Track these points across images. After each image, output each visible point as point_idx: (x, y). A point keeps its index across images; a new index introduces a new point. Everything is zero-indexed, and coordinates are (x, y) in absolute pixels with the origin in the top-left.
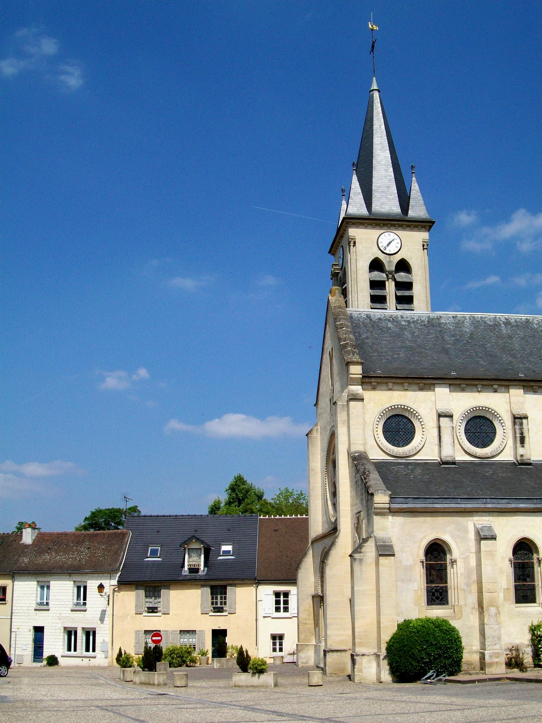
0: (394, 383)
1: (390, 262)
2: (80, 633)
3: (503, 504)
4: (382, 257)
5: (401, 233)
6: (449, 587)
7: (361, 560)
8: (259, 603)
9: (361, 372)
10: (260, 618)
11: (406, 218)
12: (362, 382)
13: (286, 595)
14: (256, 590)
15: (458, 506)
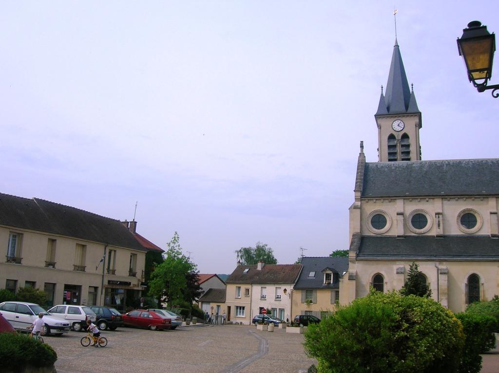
2: (278, 310)
5: (404, 119)
7: (343, 281)
11: (390, 113)
15: (389, 258)
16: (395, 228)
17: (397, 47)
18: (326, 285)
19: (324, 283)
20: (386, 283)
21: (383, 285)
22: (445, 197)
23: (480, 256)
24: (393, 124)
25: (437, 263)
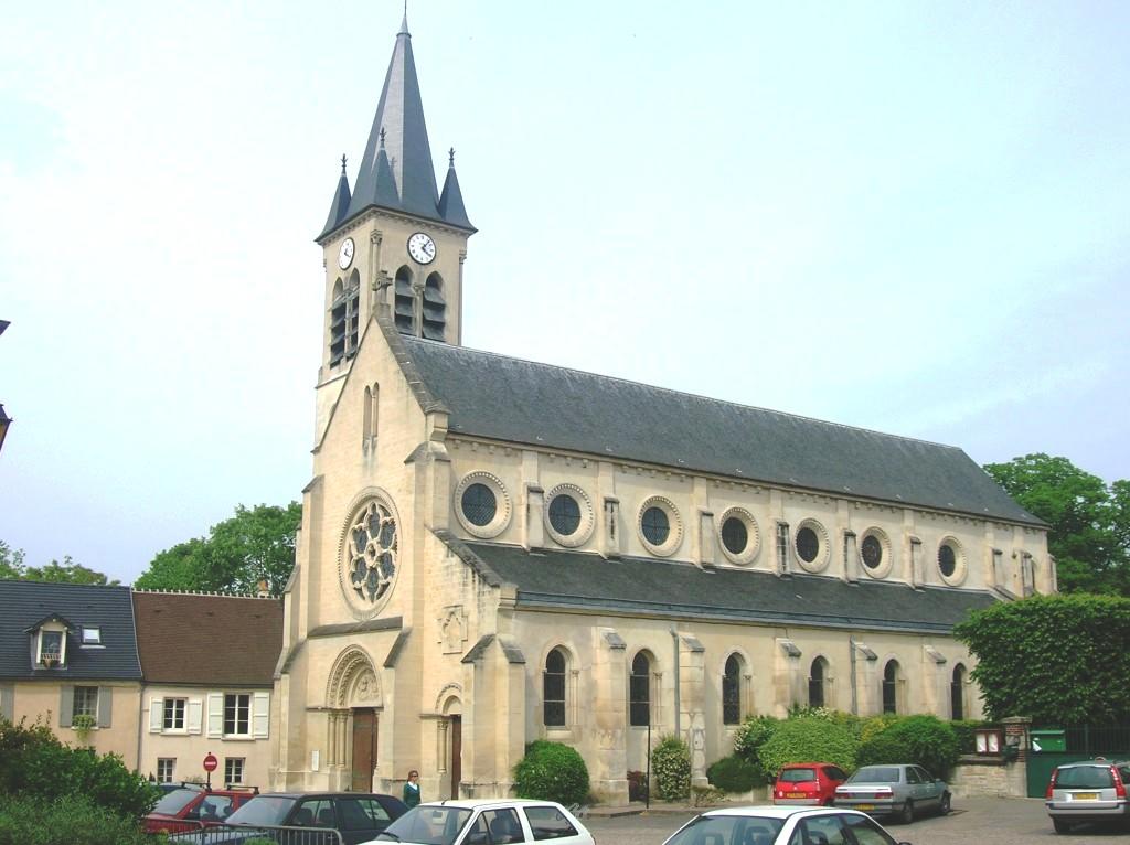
0: (480, 444)
1: (420, 274)
3: (627, 609)
4: (411, 264)
6: (566, 705)
8: (145, 714)
9: (446, 425)
10: (145, 736)
12: (446, 439)
13: (181, 704)
14: (142, 696)
16: (764, 555)
17: (405, 38)
18: (43, 668)
19: (38, 661)
20: (576, 673)
21: (648, 679)
22: (621, 462)
23: (925, 626)
24: (411, 243)
25: (675, 624)
